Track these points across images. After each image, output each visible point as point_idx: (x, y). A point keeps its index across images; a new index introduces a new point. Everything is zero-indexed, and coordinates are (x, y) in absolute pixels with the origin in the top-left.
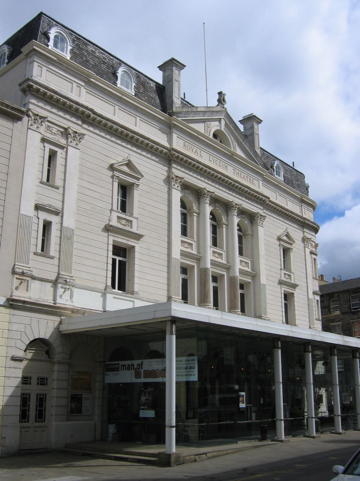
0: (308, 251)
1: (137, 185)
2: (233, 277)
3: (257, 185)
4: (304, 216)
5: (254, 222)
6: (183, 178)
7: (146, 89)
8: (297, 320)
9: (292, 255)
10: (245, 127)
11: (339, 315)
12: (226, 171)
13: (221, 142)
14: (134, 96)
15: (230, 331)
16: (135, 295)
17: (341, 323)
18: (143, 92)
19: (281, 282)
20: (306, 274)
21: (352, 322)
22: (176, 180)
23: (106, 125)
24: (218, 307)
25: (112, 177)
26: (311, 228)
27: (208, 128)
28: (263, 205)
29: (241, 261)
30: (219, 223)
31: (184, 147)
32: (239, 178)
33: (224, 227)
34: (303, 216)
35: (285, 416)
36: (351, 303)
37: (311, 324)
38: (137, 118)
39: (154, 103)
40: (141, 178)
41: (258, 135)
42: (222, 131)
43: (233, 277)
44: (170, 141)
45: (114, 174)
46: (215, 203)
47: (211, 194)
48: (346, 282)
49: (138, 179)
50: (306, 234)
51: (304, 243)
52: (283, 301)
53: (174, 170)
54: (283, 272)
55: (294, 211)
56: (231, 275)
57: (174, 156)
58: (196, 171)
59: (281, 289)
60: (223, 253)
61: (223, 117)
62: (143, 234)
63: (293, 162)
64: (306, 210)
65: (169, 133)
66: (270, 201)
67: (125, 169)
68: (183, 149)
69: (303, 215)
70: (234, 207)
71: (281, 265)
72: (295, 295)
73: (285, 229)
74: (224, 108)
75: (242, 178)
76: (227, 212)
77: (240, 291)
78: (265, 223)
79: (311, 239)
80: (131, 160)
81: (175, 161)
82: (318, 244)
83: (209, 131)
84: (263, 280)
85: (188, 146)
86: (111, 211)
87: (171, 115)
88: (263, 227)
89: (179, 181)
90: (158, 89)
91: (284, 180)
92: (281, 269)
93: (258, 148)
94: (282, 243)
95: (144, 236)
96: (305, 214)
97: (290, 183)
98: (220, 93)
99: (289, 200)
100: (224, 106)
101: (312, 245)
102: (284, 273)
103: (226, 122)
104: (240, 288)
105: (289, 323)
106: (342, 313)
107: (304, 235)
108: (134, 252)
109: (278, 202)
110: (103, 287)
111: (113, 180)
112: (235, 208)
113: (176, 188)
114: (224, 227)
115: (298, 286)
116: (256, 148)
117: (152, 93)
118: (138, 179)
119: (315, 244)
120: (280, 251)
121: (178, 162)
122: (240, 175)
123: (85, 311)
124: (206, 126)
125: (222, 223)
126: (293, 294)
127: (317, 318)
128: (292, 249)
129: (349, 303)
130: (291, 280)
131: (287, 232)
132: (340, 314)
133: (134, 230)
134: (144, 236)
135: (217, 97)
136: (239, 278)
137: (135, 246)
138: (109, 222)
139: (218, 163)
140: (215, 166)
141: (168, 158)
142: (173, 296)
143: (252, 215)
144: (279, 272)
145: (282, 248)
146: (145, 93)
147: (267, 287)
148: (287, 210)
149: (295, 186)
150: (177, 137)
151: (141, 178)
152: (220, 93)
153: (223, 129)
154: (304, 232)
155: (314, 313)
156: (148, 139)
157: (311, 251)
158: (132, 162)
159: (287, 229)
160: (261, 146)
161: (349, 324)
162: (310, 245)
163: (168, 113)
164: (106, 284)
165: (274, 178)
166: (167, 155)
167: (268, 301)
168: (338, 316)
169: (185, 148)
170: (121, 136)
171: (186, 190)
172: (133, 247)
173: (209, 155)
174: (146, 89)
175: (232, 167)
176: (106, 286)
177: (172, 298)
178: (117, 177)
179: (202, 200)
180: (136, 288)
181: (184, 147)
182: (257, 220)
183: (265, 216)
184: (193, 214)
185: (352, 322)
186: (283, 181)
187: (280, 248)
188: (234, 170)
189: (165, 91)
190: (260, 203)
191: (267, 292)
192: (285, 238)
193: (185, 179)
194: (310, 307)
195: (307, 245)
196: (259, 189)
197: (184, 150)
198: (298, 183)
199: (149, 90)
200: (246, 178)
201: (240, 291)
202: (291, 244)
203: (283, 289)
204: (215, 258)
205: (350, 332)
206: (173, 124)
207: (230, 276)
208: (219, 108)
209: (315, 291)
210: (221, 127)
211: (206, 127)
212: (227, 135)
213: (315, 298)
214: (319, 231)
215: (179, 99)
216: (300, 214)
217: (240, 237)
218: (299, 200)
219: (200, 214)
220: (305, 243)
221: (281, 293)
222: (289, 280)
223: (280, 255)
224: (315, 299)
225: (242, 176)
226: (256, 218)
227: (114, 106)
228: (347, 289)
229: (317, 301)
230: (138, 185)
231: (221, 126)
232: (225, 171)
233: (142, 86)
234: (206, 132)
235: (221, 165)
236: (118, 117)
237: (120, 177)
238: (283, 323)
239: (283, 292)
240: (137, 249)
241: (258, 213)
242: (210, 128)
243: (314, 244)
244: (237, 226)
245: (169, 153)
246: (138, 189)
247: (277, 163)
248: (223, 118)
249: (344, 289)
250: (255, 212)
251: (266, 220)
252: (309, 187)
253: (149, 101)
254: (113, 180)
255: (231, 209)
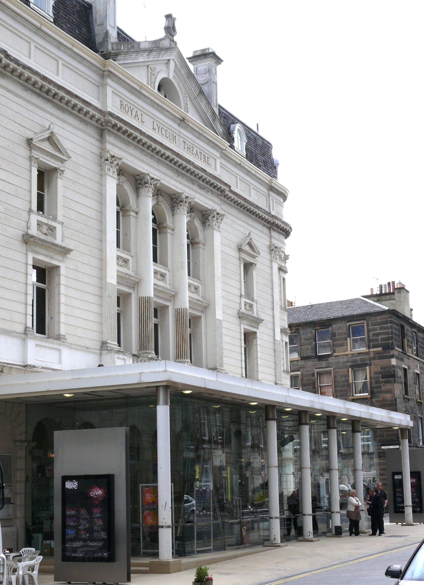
0: (275, 267)
1: (61, 170)
2: (182, 309)
3: (213, 166)
4: (273, 213)
5: (207, 224)
6: (121, 159)
7: (67, 10)
8: (260, 374)
9: (255, 273)
10: (196, 69)
11: (298, 361)
12: (175, 145)
13: (165, 97)
14: (52, 22)
15: (222, 398)
16: (62, 340)
17: (299, 373)
18: (64, 16)
19: (240, 315)
20: (273, 303)
21: (317, 373)
22: (112, 162)
23: (20, 76)
24: (158, 355)
25: (31, 158)
26: (281, 232)
27: (152, 77)
28: (220, 197)
29: (156, 272)
30: (160, 226)
31: (121, 108)
32: (191, 155)
33: (169, 233)
34: (270, 212)
35: (282, 511)
36: (317, 342)
37: (277, 379)
38: (32, 44)
39: (78, 34)
40: (66, 160)
41: (216, 84)
42: (170, 80)
43: (182, 309)
44: (103, 98)
45: (33, 154)
46: (157, 195)
47: (155, 182)
48: (309, 308)
49: (63, 161)
50: (274, 241)
51: (271, 254)
52: (243, 345)
53: (109, 147)
54: (243, 300)
55: (260, 205)
56: (178, 306)
57: (109, 124)
58: (136, 146)
59: (240, 326)
60: (167, 272)
61: (173, 57)
62: (71, 247)
63: (257, 125)
64: (274, 202)
65: (101, 86)
66: (231, 191)
67: (46, 146)
68: (119, 112)
69: (271, 210)
70: (184, 202)
71: (241, 290)
72: (258, 335)
73: (247, 234)
74: (173, 41)
75: (195, 155)
76: (173, 209)
77: (154, 320)
78: (222, 225)
79: (281, 248)
80: (54, 131)
81: (110, 131)
82: (289, 255)
83: (153, 80)
84: (219, 315)
85: (126, 105)
86: (30, 213)
87: (106, 56)
88: (220, 232)
89: (115, 163)
90: (82, 9)
91: (246, 155)
92: (241, 296)
93: (215, 105)
94: (244, 256)
95: (72, 250)
96: (273, 210)
97: (254, 159)
98: (169, 17)
99: (276, 201)
100: (174, 37)
101: (280, 257)
102: (245, 302)
103: (176, 65)
104: (154, 317)
105: (398, 409)
106: (303, 358)
107: (271, 242)
108: (255, 338)
109: (34, 63)
110: (20, 329)
111: (31, 163)
112: (186, 203)
113: (112, 175)
114: (169, 233)
115: (72, 253)
116: (214, 105)
117: (75, 17)
118: (63, 161)
119: (285, 255)
120: (31, 171)
121: (113, 133)
122: (192, 150)
123: (4, 366)
124: (149, 73)
125: (165, 226)
126: (255, 333)
127: (285, 369)
128: (256, 264)
129: (314, 343)
130: (253, 313)
131: (52, 133)
132: (300, 359)
133: (58, 241)
134: (72, 250)
135: (163, 22)
136: (189, 311)
137: (59, 267)
138: (27, 230)
139: (164, 132)
140: (160, 137)
141: (100, 126)
142: (108, 341)
143: (205, 213)
144: (237, 300)
145: (243, 263)
146: (67, 18)
147: (224, 324)
148: (252, 204)
149: (260, 165)
150: (113, 92)
151: (66, 160)
152: (169, 17)
153: (171, 78)
154: (271, 237)
155: (282, 363)
156: (36, 73)
157: (280, 267)
158: (56, 134)
159: (250, 235)
160: (220, 102)
161: (313, 374)
162: (278, 257)
163: (100, 53)
164: (26, 324)
165: (234, 151)
166: (100, 122)
167: (225, 346)
168: (296, 362)
169: (122, 110)
170: (40, 92)
171: (121, 176)
172: (57, 267)
173: (153, 120)
174: (67, 10)
175: (152, 118)
176: (26, 327)
177: (108, 343)
178: (36, 159)
179: (177, 211)
180: (63, 330)
181: (121, 108)
182: (211, 220)
183: (223, 215)
184: (128, 214)
185: (317, 373)
186: (245, 157)
187: (31, 166)
188: (201, 153)
189: (92, 13)
190: (216, 193)
191: (224, 331)
192: (247, 248)
193: (124, 160)
194: (276, 352)
195: (217, 226)
196: (215, 172)
197: (120, 113)
198: (264, 159)
199: (71, 11)
200: (199, 154)
201: (154, 320)
202: (254, 257)
203: (243, 326)
204: (157, 280)
205: (314, 388)
206: (107, 72)
207: (179, 308)
208: (166, 43)
209: (284, 329)
210: (169, 74)
211: (150, 74)
212: (176, 85)
213: (283, 340)
214: (291, 233)
215: (114, 28)
216: (267, 210)
217: (154, 231)
218: (265, 187)
219: (139, 213)
220: (273, 255)
221: (241, 333)
222: (250, 313)
223: (30, 181)
224: (283, 341)
225: (195, 152)
226: (210, 217)
227: (30, 43)
228: (311, 319)
229: (286, 343)
230: (63, 171)
231: (169, 72)
232: (172, 145)
233: (61, 5)
234: (150, 83)
235: (168, 135)
236: (35, 61)
237: (41, 159)
238: (242, 377)
239: (243, 332)
240: (63, 271)
241: (215, 210)
242: (155, 76)
243: (283, 256)
244: (152, 215)
245: (102, 120)
246: (63, 178)
247: (239, 128)
248: (173, 59)
249: (306, 320)
250: (210, 208)
251: (224, 220)
252: (279, 164)
253: (73, 32)
254: (31, 163)
255: (179, 205)
